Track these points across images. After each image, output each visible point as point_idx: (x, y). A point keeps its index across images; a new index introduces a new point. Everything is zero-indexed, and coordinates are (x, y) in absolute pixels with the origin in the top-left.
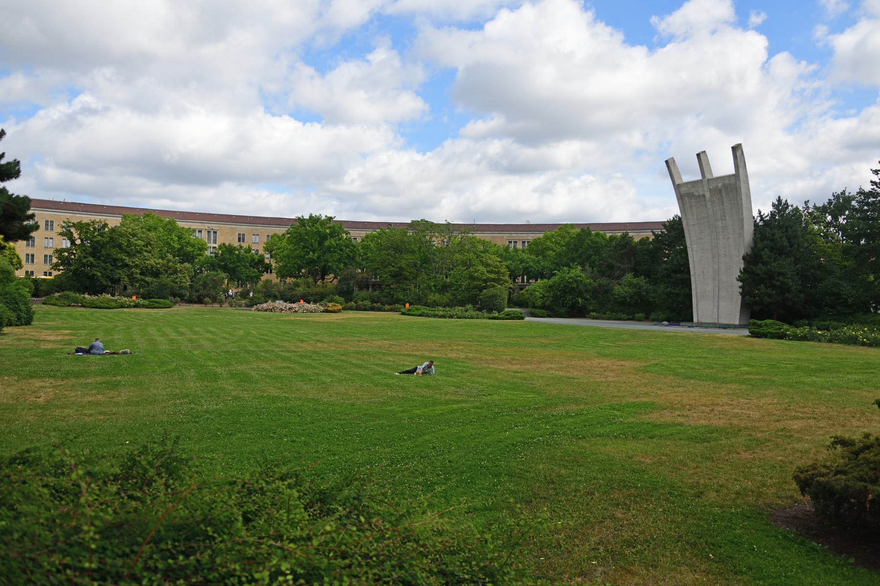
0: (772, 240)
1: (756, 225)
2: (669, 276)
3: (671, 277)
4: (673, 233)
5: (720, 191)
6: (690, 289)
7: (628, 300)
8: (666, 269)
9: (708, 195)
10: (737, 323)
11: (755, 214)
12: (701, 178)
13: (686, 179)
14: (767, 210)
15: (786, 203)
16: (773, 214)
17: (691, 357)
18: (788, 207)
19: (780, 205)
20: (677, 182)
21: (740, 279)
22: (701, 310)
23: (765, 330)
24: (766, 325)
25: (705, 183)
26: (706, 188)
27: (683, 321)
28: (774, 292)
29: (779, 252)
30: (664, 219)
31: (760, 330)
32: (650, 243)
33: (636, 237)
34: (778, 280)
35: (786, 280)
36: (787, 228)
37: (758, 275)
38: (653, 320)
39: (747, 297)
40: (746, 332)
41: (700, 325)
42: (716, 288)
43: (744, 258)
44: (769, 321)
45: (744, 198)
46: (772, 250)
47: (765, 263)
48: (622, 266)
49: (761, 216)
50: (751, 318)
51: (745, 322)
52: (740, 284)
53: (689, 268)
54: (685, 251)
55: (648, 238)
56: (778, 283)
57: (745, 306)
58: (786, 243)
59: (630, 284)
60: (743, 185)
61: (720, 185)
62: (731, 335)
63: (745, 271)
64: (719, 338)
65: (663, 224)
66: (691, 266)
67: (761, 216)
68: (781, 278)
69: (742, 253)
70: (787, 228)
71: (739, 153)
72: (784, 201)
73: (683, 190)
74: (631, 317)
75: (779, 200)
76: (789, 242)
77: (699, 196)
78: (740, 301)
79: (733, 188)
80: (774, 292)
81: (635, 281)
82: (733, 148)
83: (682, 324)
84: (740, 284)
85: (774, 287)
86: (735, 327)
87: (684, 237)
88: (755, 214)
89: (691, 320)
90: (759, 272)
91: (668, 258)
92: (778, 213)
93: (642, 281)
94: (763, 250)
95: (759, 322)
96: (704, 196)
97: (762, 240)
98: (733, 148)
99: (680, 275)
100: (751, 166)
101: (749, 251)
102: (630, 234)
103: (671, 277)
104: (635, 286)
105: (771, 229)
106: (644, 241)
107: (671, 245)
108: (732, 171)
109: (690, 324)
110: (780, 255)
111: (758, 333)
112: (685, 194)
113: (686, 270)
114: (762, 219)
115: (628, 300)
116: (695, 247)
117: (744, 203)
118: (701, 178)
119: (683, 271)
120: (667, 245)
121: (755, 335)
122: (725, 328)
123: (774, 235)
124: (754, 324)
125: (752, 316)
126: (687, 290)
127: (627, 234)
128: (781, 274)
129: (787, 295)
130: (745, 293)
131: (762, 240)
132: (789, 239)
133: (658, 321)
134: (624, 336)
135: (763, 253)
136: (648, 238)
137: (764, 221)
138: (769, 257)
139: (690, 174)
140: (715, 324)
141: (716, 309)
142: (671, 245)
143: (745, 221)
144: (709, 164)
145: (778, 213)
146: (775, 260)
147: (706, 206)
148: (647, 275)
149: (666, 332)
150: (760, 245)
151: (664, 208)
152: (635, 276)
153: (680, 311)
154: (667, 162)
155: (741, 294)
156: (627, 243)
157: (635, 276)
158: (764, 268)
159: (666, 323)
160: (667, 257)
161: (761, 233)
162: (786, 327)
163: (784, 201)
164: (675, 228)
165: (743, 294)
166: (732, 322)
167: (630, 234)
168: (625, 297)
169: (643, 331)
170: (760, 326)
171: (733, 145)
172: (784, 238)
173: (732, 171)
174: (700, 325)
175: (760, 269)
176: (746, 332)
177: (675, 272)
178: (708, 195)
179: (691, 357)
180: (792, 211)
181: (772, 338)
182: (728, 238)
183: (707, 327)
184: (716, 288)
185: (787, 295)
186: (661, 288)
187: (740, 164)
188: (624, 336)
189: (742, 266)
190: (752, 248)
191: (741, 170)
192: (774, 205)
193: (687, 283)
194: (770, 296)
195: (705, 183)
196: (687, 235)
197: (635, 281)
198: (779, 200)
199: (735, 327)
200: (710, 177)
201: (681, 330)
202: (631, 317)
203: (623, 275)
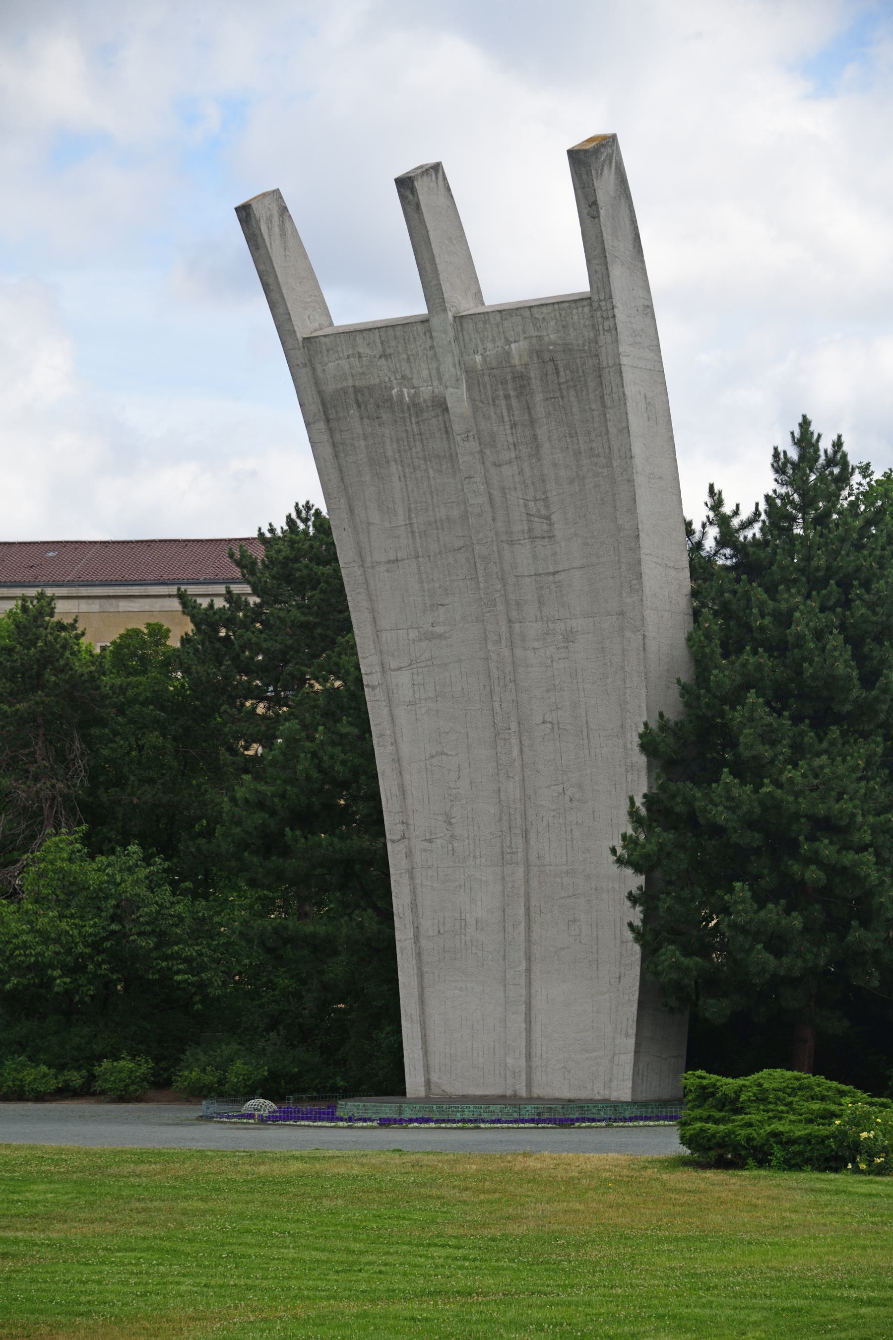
0: (779, 648)
1: (700, 567)
2: (270, 844)
3: (286, 852)
4: (291, 609)
5: (521, 380)
6: (387, 916)
7: (61, 982)
8: (261, 805)
9: (458, 399)
10: (623, 1091)
11: (696, 510)
12: (420, 309)
13: (350, 307)
14: (750, 487)
15: (838, 456)
16: (777, 513)
17: (391, 1295)
18: (843, 479)
19: (810, 467)
20: (303, 328)
21: (633, 857)
22: (449, 1025)
23: (754, 1124)
24: (761, 1098)
25: (444, 335)
26: (449, 367)
27: (351, 1092)
28: (797, 921)
29: (815, 707)
30: (245, 530)
31: (734, 1127)
32: (171, 660)
33: (98, 623)
34: (814, 859)
35: (849, 857)
36: (845, 585)
37: (718, 831)
38: (197, 1093)
39: (671, 953)
40: (667, 1141)
41: (444, 1111)
42: (518, 941)
43: (648, 745)
44: (774, 1078)
45: (636, 422)
46: (779, 699)
47: (750, 771)
48: (22, 792)
49: (723, 521)
50: (691, 1066)
51: (654, 1089)
52: (635, 881)
53: (375, 797)
54: (352, 705)
55: (158, 633)
56: (813, 874)
57: (661, 997)
58: (843, 664)
59: (70, 890)
60: (630, 357)
61: (518, 349)
62: (595, 1159)
63: (656, 813)
64: (534, 1179)
65: (236, 552)
66: (387, 787)
67: (723, 521)
68: (827, 849)
69: (639, 718)
70: (845, 585)
71: (604, 188)
72: (826, 445)
73: (334, 368)
74: (76, 1078)
75: (805, 439)
76: (860, 658)
77: (416, 408)
78: (636, 971)
79: (580, 365)
80: (797, 921)
81: (93, 872)
82: (575, 156)
83: (347, 1107)
84: (635, 881)
85: (792, 893)
86: (612, 1114)
87: (347, 626)
88: (696, 510)
89: (392, 1083)
90: (722, 816)
91: (267, 741)
92: (803, 508)
93: (126, 871)
94: (735, 698)
95: (728, 1084)
96: (441, 406)
97: (731, 648)
98: (575, 156)
99: (331, 837)
100: (667, 257)
101: (674, 711)
102: (64, 610)
103: (286, 852)
104: (96, 899)
105: (771, 591)
106: (135, 651)
107: (279, 672)
108: (578, 281)
109: (387, 1107)
110: (820, 723)
111: (723, 1143)
112: (346, 388)
113: (362, 809)
114: (727, 538)
115: (61, 982)
116: (403, 679)
117: (637, 449)
118: (420, 309)
119: (345, 815)
120: (261, 670)
121: (715, 1153)
122: (565, 1123)
123: (784, 619)
124: (705, 1094)
125: (694, 1060)
126: (367, 918)
127: (46, 606)
128: (825, 826)
129: (856, 933)
130: (659, 931)
131: (731, 648)
132: (855, 641)
133: (221, 1093)
134: (38, 1192)
135: (738, 715)
136: (158, 633)
137: (740, 549)
138: (769, 737)
139: (369, 287)
140: (513, 1100)
141: (518, 1022)
142: (279, 672)
143: (646, 542)
144: (529, 301)
145: (803, 508)
146: (798, 750)
147: (453, 458)
148: (162, 836)
149: (262, 1158)
150: (724, 674)
151: (242, 470)
152: (95, 846)
153: (334, 1039)
154: (245, 213)
155: (639, 936)
156: (47, 660)
157: (95, 846)
158: (743, 792)
159: (264, 1106)
160: (263, 737)
161: (725, 612)
162: (855, 1102)
163: (826, 445)
164: (297, 573)
165: (650, 938)
166: (597, 1091)
167: (64, 610)
168: (39, 968)
169: (141, 1157)
170: (732, 1105)
171: (575, 140)
172: (835, 640)
173: (578, 281)
174: (444, 1111)
175: (726, 800)
176: (667, 1141)
177: (304, 819)
178: (458, 399)
179: (391, 1295)
180: (868, 496)
181: (792, 1165)
182: (569, 637)
183: (476, 1122)
184: (518, 941)
185: (856, 933)
186: (236, 911)
187: (616, 245)
188: (38, 1192)
189: (641, 787)
190: (685, 690)
191: (618, 273)
192: (780, 464)
193: (365, 881)
194: (777, 944)
195: (444, 335)
196: (358, 617)
197: (93, 872)
198: (805, 439)
199: (612, 1114)
200: (467, 307)
201: (341, 1145)
202: (76, 1078)
203: (30, 840)
